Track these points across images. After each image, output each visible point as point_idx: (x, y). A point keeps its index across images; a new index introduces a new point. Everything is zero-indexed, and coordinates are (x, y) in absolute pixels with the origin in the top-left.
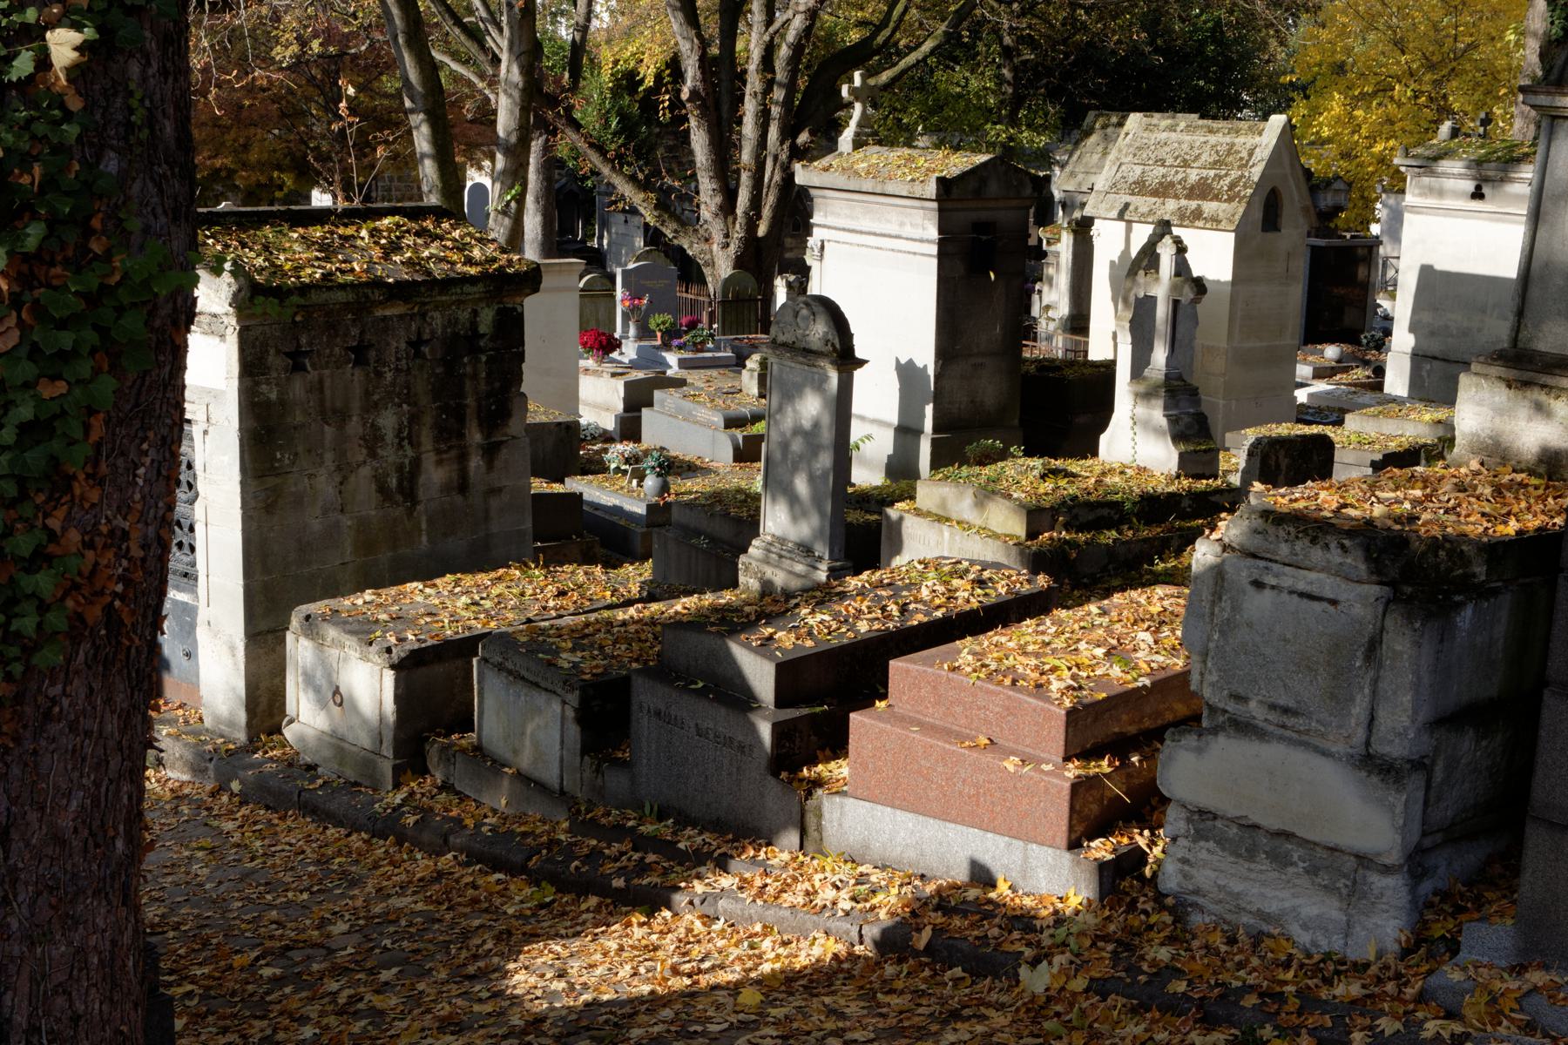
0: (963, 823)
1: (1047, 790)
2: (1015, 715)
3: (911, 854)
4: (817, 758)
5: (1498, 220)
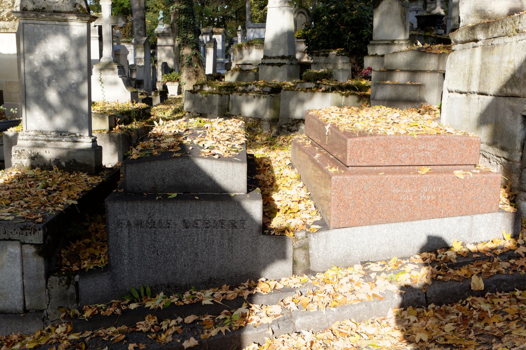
0: (426, 218)
1: (486, 183)
2: (446, 149)
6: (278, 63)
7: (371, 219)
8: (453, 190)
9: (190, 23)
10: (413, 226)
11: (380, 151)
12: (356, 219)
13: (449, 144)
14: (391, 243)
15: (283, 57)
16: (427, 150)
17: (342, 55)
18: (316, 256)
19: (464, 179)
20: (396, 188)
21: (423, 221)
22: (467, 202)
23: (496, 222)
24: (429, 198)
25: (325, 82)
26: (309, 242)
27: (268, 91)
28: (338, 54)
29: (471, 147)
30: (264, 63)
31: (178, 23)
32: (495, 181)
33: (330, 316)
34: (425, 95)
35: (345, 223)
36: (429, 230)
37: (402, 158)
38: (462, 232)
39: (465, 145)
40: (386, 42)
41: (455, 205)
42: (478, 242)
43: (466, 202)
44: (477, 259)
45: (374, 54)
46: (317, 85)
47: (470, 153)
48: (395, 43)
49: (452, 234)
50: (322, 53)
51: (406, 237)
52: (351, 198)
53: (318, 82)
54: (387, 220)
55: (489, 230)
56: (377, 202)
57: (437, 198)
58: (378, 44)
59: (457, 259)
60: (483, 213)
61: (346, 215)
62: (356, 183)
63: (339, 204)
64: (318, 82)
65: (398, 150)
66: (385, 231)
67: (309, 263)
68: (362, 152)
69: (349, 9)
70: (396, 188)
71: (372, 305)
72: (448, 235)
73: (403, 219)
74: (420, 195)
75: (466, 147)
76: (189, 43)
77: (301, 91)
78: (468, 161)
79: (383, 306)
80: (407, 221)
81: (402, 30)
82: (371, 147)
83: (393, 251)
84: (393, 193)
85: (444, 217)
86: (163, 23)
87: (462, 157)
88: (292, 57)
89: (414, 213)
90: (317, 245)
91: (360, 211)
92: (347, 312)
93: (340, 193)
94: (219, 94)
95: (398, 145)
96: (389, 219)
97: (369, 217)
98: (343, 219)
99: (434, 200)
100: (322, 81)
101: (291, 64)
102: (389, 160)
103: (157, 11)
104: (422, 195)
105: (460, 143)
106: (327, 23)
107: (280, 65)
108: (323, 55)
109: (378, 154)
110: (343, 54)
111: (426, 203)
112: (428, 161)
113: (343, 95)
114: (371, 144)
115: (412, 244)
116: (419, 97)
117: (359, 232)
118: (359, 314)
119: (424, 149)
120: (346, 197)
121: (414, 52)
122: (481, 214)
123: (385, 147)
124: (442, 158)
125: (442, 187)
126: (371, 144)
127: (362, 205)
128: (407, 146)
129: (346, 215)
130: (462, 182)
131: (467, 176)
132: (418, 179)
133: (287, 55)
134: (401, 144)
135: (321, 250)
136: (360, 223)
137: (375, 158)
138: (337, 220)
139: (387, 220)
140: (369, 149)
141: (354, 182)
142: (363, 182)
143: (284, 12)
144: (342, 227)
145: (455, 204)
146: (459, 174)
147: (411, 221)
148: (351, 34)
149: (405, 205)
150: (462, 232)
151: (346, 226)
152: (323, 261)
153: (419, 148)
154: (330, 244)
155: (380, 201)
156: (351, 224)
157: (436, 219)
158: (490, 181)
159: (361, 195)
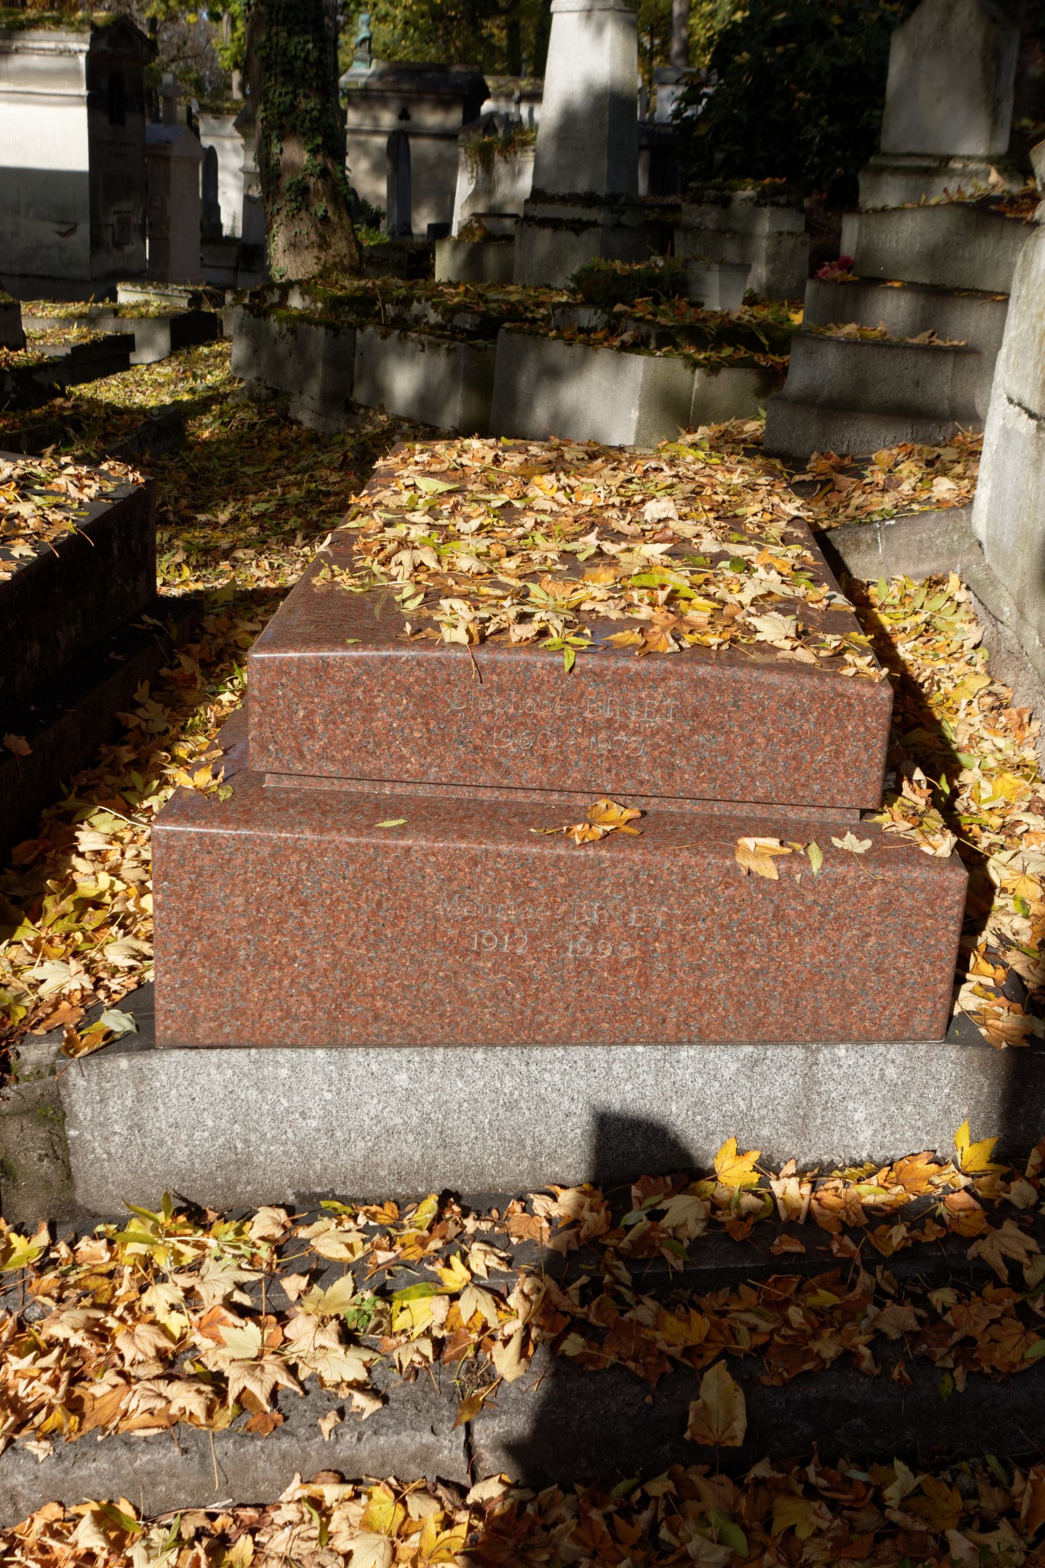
0: (592, 1038)
1: (888, 906)
2: (720, 728)
3: (410, 1150)
4: (1001, 1204)
5: (17, 102)
6: (573, 221)
7: (335, 1020)
8: (722, 927)
9: (306, 60)
10: (533, 1067)
11: (398, 716)
12: (268, 1016)
13: (735, 704)
14: (429, 1127)
15: (589, 200)
16: (624, 727)
17: (775, 204)
18: (99, 1150)
19: (779, 882)
20: (450, 898)
21: (579, 1053)
22: (793, 986)
23: (926, 1085)
24: (608, 953)
25: (643, 307)
26: (63, 1092)
27: (468, 327)
28: (761, 200)
29: (843, 728)
30: (533, 218)
31: (263, 59)
32: (931, 904)
33: (21, 1479)
34: (977, 391)
35: (221, 1025)
36: (607, 1090)
37: (504, 753)
38: (764, 1112)
39: (812, 718)
40: (925, 163)
41: (730, 994)
42: (836, 1159)
43: (785, 984)
44: (785, 1264)
45: (879, 205)
46: (613, 321)
47: (838, 753)
48: (954, 170)
49: (714, 1116)
50: (712, 193)
51: (501, 1111)
52: (243, 922)
53: (619, 308)
54: (412, 1030)
55: (891, 1117)
56: (362, 951)
57: (646, 955)
58: (896, 171)
59: (697, 1245)
60: (867, 1039)
61: (221, 995)
62: (262, 861)
63: (187, 943)
64: (619, 308)
65: (485, 719)
66: (402, 1079)
67: (69, 1176)
68: (312, 712)
69: (838, 26)
70: (450, 898)
71: (216, 1451)
72: (699, 1118)
73: (485, 1034)
74: (564, 935)
75: (817, 723)
76: (299, 129)
77: (555, 338)
78: (823, 790)
79: (261, 1464)
80: (505, 1044)
81: (982, 123)
82: (359, 693)
83: (440, 1161)
84: (436, 918)
85: (680, 1043)
86: (367, 57)
87: (797, 769)
88: (622, 200)
89: (535, 1012)
90: (98, 1108)
91: (286, 983)
92: (97, 1471)
93: (188, 899)
94: (329, 326)
95: (487, 693)
96: (420, 1030)
97: (329, 1013)
98: (208, 1009)
99: (630, 962)
100: (633, 306)
101: (618, 226)
102: (442, 758)
103: (387, 15)
104: (575, 938)
105: (790, 704)
106: (747, 80)
107: (578, 227)
108: (714, 202)
109: (389, 729)
110: (783, 199)
111: (592, 973)
112: (632, 776)
113: (695, 365)
114: (355, 682)
115: (529, 1142)
116: (951, 400)
117: (284, 1072)
118: (154, 1485)
119: (610, 721)
120: (219, 917)
121: (960, 211)
122: (858, 1042)
123: (423, 698)
124: (700, 767)
125: (671, 908)
126: (355, 682)
127: (294, 959)
128: (529, 702)
129: (221, 995)
130: (766, 894)
131: (795, 866)
132: (555, 865)
133: (603, 191)
134: (501, 690)
135: (117, 1128)
136: (286, 1034)
137: (378, 745)
138: (185, 1014)
139: (412, 1030)
140: (347, 702)
141: (252, 857)
142: (294, 858)
143: (600, 29)
144: (208, 1042)
145: (734, 989)
146: (758, 854)
147: (524, 1044)
148: (830, 123)
149: (495, 973)
150: (764, 1112)
151: (221, 1041)
152: (129, 1177)
153: (588, 715)
154: (157, 1109)
155: (375, 946)
156: (246, 1033)
157: (640, 1049)
158: (909, 903)
159: (288, 916)
